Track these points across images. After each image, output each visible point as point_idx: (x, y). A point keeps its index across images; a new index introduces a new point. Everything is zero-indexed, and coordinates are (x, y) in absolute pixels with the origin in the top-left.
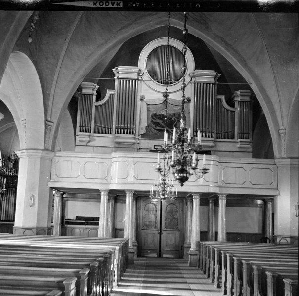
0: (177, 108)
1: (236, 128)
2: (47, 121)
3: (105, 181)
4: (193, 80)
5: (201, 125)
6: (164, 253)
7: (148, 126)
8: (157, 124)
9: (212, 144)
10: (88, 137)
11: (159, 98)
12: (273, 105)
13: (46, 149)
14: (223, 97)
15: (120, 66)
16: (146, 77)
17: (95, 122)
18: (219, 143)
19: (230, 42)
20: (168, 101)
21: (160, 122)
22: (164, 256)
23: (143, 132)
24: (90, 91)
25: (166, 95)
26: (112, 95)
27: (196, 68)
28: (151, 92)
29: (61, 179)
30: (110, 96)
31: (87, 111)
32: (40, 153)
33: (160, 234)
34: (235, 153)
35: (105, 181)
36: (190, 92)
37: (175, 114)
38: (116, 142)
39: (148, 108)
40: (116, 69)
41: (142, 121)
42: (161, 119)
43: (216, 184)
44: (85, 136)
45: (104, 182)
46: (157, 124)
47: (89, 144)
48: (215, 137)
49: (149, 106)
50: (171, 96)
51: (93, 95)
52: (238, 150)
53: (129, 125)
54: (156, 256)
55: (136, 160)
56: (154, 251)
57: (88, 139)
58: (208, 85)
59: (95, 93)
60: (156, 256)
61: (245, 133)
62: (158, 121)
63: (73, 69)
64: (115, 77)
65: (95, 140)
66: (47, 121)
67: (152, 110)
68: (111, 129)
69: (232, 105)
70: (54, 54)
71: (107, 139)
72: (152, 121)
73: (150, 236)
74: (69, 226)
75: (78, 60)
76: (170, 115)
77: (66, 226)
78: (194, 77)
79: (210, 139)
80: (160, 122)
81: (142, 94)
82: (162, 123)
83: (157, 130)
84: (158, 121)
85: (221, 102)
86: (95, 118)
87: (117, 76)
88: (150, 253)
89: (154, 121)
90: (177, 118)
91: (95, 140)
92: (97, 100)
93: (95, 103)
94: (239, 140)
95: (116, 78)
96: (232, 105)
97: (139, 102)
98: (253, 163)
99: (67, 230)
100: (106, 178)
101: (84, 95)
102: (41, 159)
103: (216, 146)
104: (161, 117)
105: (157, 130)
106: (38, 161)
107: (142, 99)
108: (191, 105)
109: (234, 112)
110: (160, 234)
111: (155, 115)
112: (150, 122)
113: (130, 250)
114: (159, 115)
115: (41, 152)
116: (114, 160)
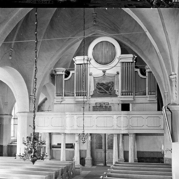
0: (111, 79)
1: (147, 88)
2: (31, 96)
3: (63, 128)
4: (120, 61)
5: (125, 88)
6: (108, 164)
7: (95, 90)
8: (100, 89)
9: (132, 99)
10: (61, 99)
11: (101, 73)
12: (160, 78)
13: (30, 112)
14: (138, 70)
15: (77, 57)
16: (93, 61)
17: (65, 90)
18: (136, 98)
19: (132, 41)
20: (105, 74)
21: (102, 87)
22: (108, 165)
23: (92, 94)
24: (61, 73)
25: (104, 72)
26: (73, 74)
27: (122, 53)
28: (95, 70)
29: (39, 128)
30: (72, 74)
31: (66, 82)
32: (26, 114)
33: (105, 152)
34: (146, 104)
35: (63, 128)
36: (119, 69)
37: (110, 82)
38: (76, 101)
39: (94, 80)
40: (75, 59)
41: (91, 87)
42: (102, 86)
43: (127, 128)
44: (59, 99)
45: (62, 129)
46: (100, 89)
47: (62, 103)
48: (134, 95)
49: (95, 78)
50: (107, 72)
51: (63, 75)
52: (148, 102)
53: (85, 91)
54: (103, 165)
55: (78, 116)
56: (101, 162)
57: (61, 100)
58: (129, 63)
59: (64, 73)
60: (103, 165)
61: (152, 92)
62: (100, 87)
63: (44, 66)
64: (54, 74)
65: (65, 100)
66: (31, 96)
67: (96, 81)
68: (73, 93)
69: (144, 75)
70: (31, 59)
71: (70, 99)
72: (97, 87)
73: (99, 153)
74: (54, 149)
75: (46, 60)
76: (107, 83)
77: (52, 149)
78: (121, 59)
79: (130, 96)
80: (102, 87)
81: (90, 72)
82: (105, 88)
83: (100, 92)
84: (100, 87)
85: (137, 73)
86: (65, 87)
87: (75, 62)
88: (100, 163)
89: (98, 87)
90: (112, 85)
91: (65, 100)
92: (66, 77)
93: (64, 79)
94: (148, 96)
95: (75, 64)
96: (144, 75)
97: (89, 77)
98: (147, 114)
99: (53, 151)
100: (63, 126)
101: (58, 75)
102: (28, 117)
103: (134, 100)
104: (102, 85)
105: (100, 92)
106: (26, 118)
107: (91, 75)
108: (120, 76)
109: (145, 79)
110: (105, 152)
111: (99, 83)
112: (96, 88)
113: (76, 167)
114: (101, 83)
115: (27, 113)
116: (67, 116)
